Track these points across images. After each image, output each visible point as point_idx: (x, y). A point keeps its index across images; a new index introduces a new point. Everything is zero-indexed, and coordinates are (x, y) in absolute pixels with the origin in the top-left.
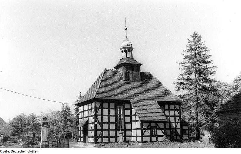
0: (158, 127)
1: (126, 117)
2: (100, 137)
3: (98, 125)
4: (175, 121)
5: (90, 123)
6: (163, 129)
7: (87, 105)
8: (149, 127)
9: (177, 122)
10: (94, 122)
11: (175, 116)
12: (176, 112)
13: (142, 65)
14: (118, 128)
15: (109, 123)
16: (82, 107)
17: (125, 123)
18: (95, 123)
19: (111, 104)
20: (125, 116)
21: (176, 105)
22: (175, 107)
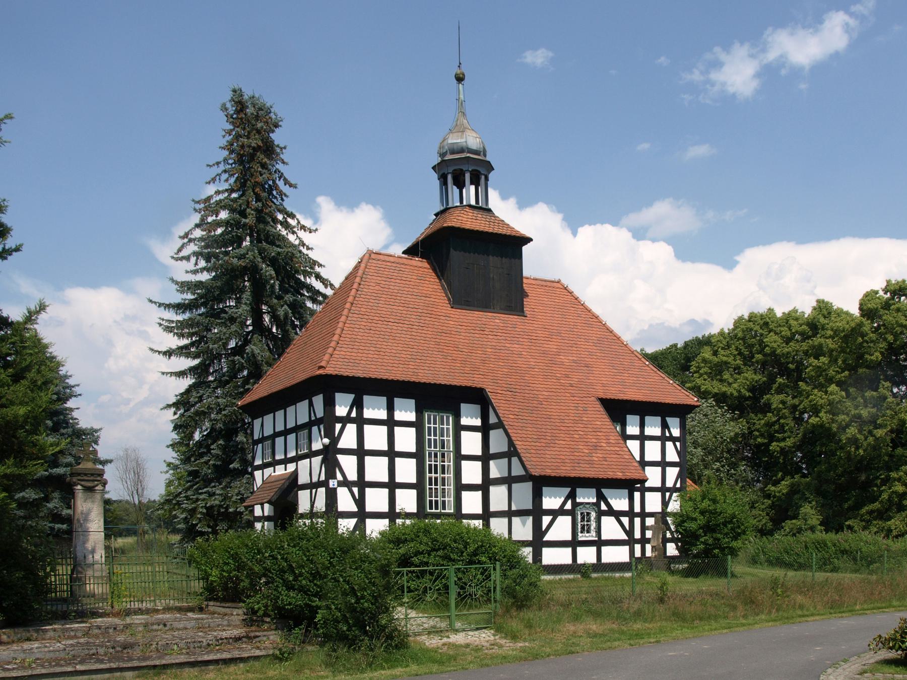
0: (604, 507)
1: (465, 464)
5: (304, 487)
7: (291, 410)
8: (568, 506)
9: (669, 490)
10: (323, 478)
11: (663, 464)
12: (669, 445)
14: (431, 508)
15: (392, 485)
16: (268, 418)
17: (460, 487)
18: (331, 486)
20: (460, 457)
21: (669, 420)
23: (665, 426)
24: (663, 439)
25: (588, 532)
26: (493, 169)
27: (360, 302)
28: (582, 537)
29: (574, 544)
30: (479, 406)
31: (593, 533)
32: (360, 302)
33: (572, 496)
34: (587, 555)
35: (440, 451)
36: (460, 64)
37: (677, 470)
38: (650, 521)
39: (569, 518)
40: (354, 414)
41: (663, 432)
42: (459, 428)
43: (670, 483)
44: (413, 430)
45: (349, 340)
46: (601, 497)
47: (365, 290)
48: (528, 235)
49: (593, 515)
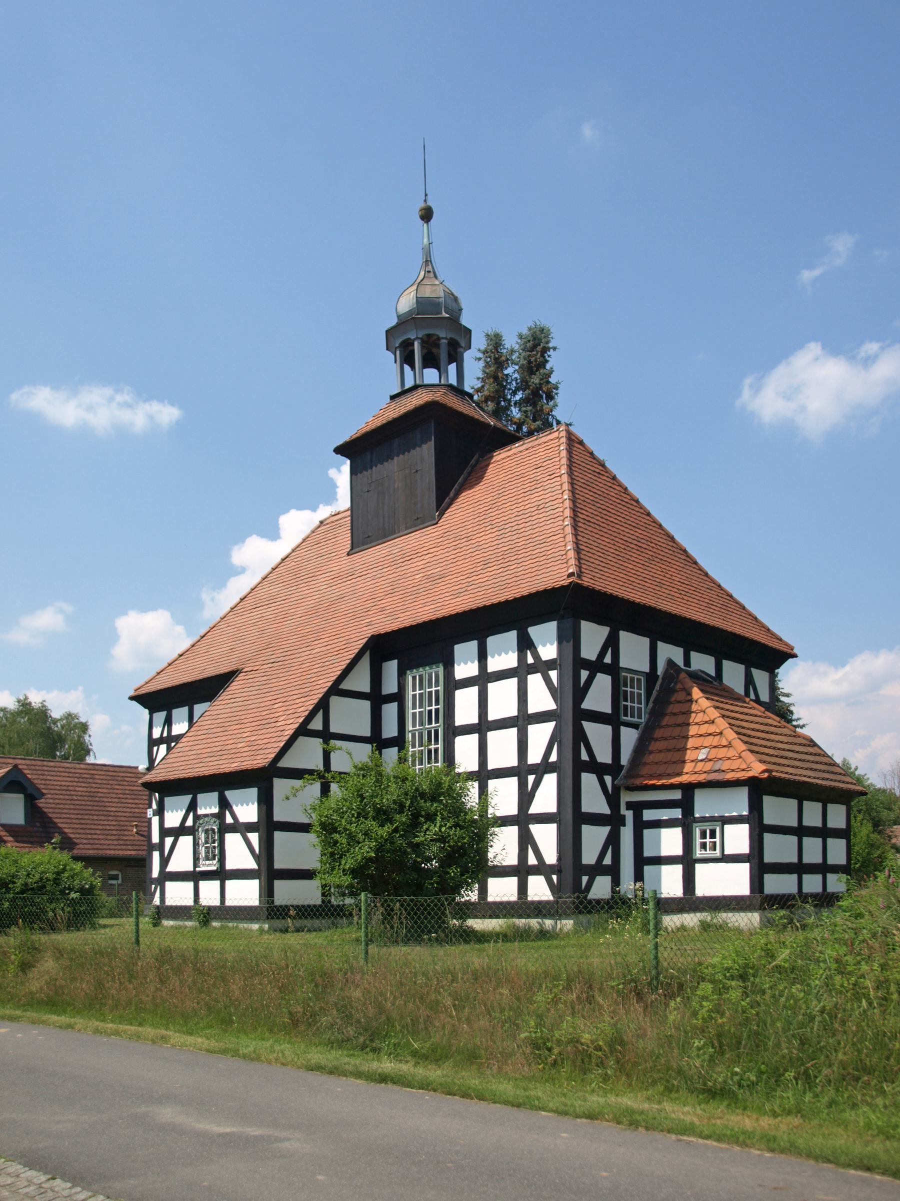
0: (229, 820)
23: (525, 644)
24: (520, 673)
33: (192, 807)
34: (210, 892)
36: (426, 195)
41: (522, 658)
42: (452, 685)
46: (224, 804)
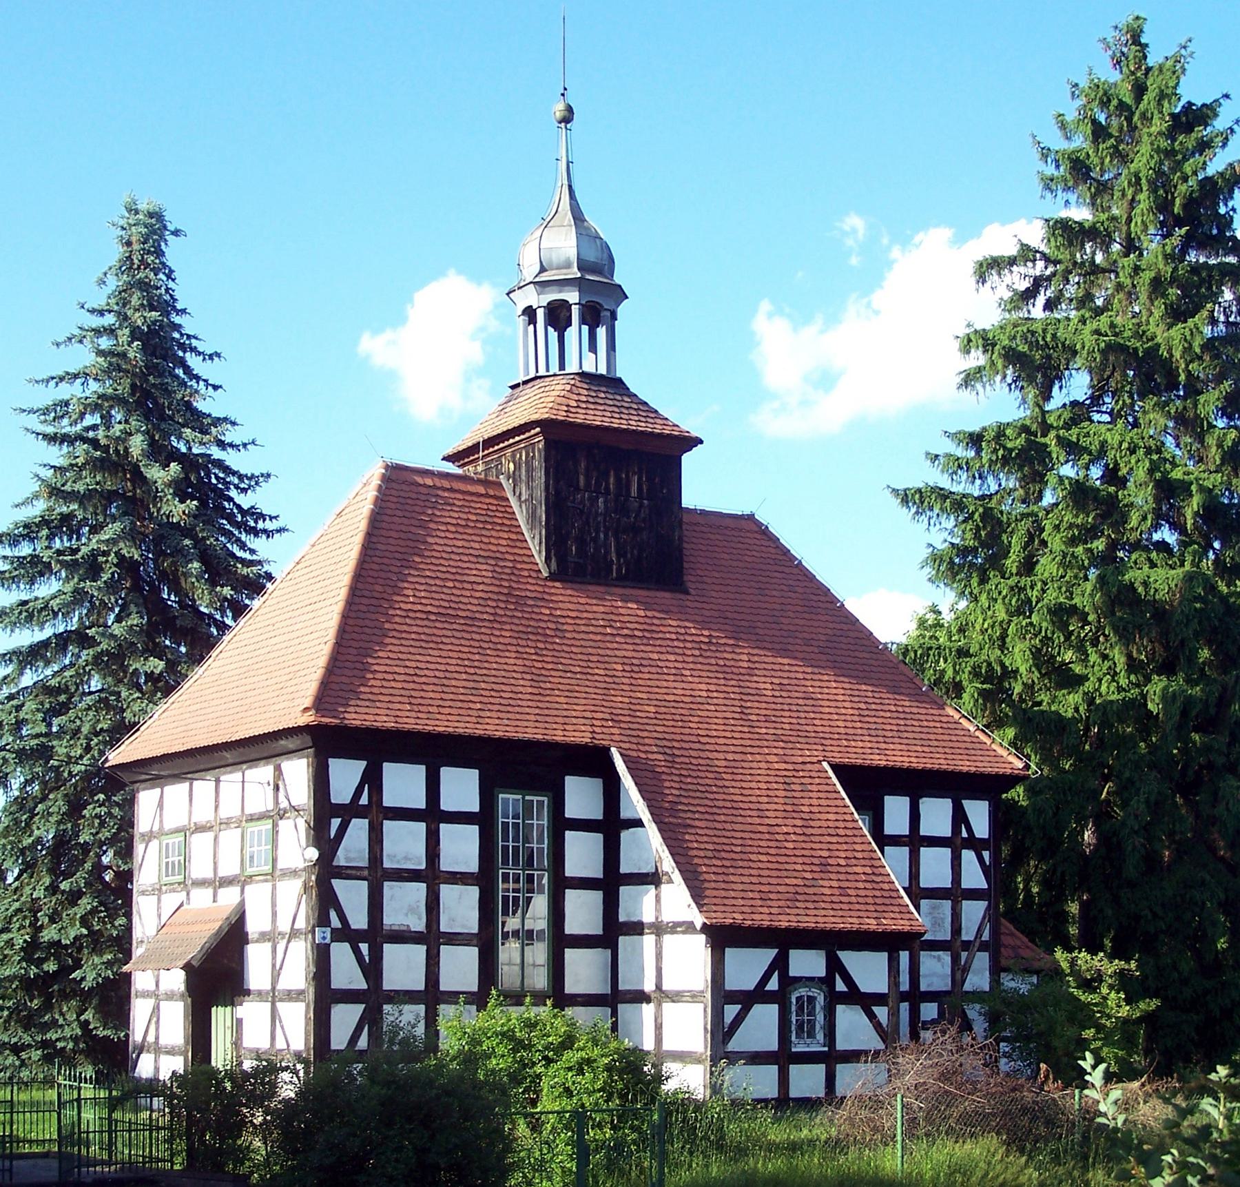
0: (840, 986)
2: (350, 811)
3: (342, 955)
4: (956, 929)
6: (880, 999)
8: (773, 985)
9: (967, 945)
13: (701, 442)
19: (448, 775)
20: (561, 884)
21: (967, 804)
22: (960, 817)
25: (811, 1034)
26: (627, 297)
27: (371, 573)
28: (798, 1047)
29: (783, 1058)
30: (600, 781)
31: (820, 1036)
32: (371, 573)
35: (523, 870)
37: (982, 905)
38: (929, 1011)
39: (774, 1008)
40: (364, 800)
42: (561, 824)
43: (968, 934)
44: (474, 830)
45: (355, 652)
47: (379, 546)
48: (695, 433)
49: (821, 1000)
